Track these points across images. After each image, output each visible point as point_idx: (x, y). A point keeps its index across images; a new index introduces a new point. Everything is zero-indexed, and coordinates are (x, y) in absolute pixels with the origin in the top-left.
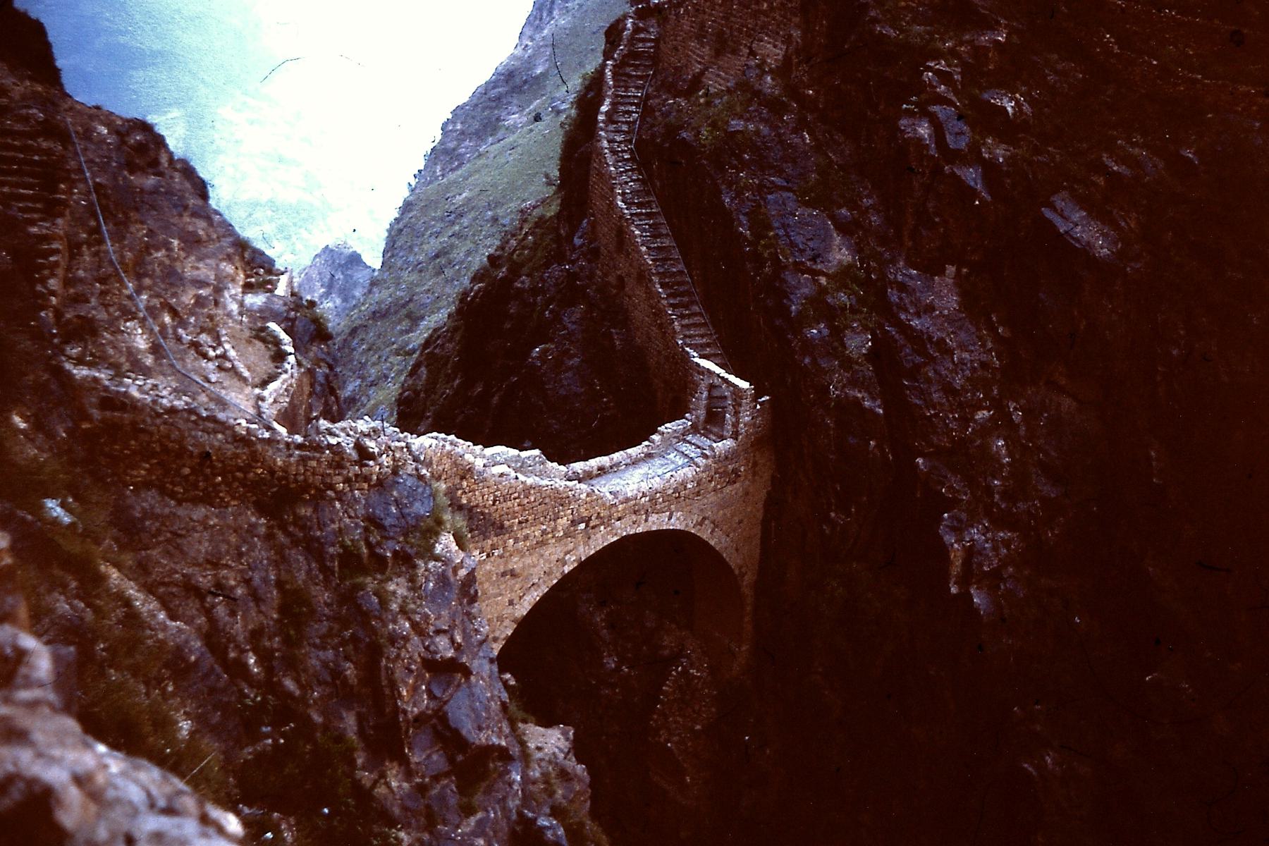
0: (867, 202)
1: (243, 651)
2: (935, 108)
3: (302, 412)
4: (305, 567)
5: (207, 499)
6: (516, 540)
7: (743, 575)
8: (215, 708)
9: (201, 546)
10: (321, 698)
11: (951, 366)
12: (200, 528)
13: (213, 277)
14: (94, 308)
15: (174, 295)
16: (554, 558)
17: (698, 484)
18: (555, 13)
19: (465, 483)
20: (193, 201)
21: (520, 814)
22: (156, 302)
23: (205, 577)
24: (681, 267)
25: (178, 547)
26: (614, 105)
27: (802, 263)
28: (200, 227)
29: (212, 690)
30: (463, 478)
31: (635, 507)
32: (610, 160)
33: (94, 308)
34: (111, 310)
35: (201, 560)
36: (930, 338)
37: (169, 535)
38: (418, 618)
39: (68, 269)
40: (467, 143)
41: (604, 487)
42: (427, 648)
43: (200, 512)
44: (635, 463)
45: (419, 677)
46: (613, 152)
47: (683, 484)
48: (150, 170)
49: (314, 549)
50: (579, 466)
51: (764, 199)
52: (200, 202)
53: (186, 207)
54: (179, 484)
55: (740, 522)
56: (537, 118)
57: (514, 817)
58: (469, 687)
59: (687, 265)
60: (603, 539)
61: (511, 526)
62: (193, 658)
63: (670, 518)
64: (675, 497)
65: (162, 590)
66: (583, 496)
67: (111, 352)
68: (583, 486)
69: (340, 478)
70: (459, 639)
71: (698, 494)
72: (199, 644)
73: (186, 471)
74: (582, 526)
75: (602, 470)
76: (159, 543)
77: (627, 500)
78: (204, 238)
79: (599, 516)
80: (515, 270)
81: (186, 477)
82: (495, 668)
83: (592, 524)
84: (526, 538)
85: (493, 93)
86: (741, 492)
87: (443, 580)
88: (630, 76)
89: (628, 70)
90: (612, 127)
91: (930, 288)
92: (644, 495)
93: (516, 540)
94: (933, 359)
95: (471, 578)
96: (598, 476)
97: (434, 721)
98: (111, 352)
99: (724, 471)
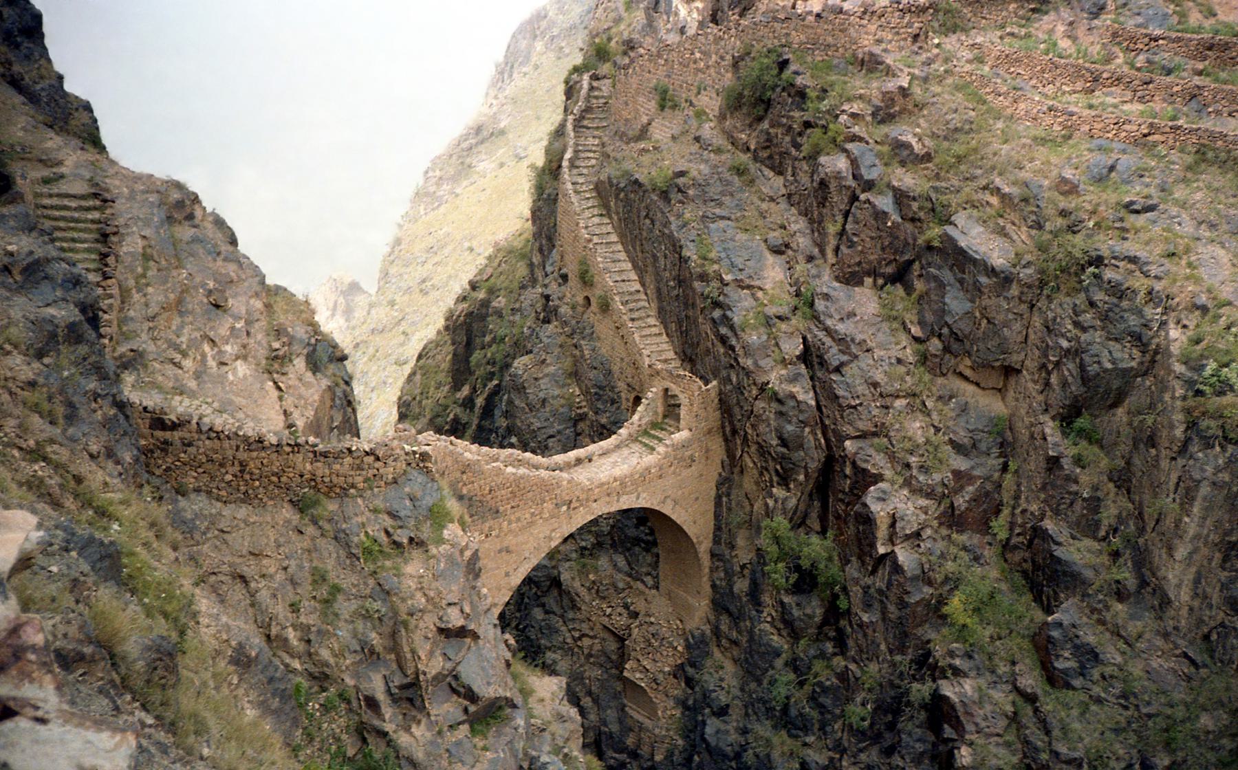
0: (794, 227)
1: (284, 628)
2: (849, 146)
3: (325, 423)
4: (334, 555)
5: (247, 499)
6: (510, 523)
7: (700, 543)
8: (274, 695)
9: (241, 540)
10: (353, 664)
11: (871, 362)
12: (242, 525)
13: (244, 312)
14: (144, 342)
15: (212, 328)
16: (541, 536)
17: (661, 469)
18: (515, 75)
19: (465, 477)
20: (225, 248)
21: (526, 754)
22: (197, 334)
23: (249, 566)
24: (638, 286)
25: (226, 542)
26: (576, 152)
27: (741, 280)
28: (231, 269)
29: (271, 680)
30: (463, 473)
31: (608, 489)
32: (574, 199)
33: (144, 342)
34: (159, 343)
35: (244, 552)
36: (853, 340)
37: (216, 532)
38: (432, 594)
39: (121, 310)
40: (445, 187)
41: (582, 475)
42: (440, 619)
43: (243, 512)
44: (604, 454)
45: (435, 644)
46: (576, 192)
47: (648, 469)
48: (187, 223)
49: (341, 538)
50: (559, 458)
51: (708, 228)
52: (231, 248)
53: (219, 254)
54: (224, 488)
55: (697, 499)
56: (502, 165)
57: (521, 756)
58: (479, 649)
59: (643, 285)
60: (582, 518)
61: (506, 510)
62: (253, 654)
63: (638, 498)
64: (643, 478)
65: (213, 578)
66: (565, 483)
67: (160, 378)
68: (565, 475)
69: (360, 479)
70: (467, 609)
71: (660, 477)
72: (257, 641)
73: (229, 477)
74: (565, 508)
75: (579, 461)
76: (208, 539)
77: (603, 484)
78: (235, 278)
79: (578, 500)
80: (492, 291)
81: (229, 483)
82: (499, 631)
83: (572, 506)
84: (518, 520)
85: (465, 145)
86: (696, 474)
87: (450, 559)
88: (588, 128)
89: (585, 123)
90: (575, 171)
91: (849, 297)
92: (615, 480)
93: (510, 523)
94: (856, 357)
95: (475, 556)
96: (575, 465)
97: (449, 679)
98: (160, 378)
99: (681, 458)
